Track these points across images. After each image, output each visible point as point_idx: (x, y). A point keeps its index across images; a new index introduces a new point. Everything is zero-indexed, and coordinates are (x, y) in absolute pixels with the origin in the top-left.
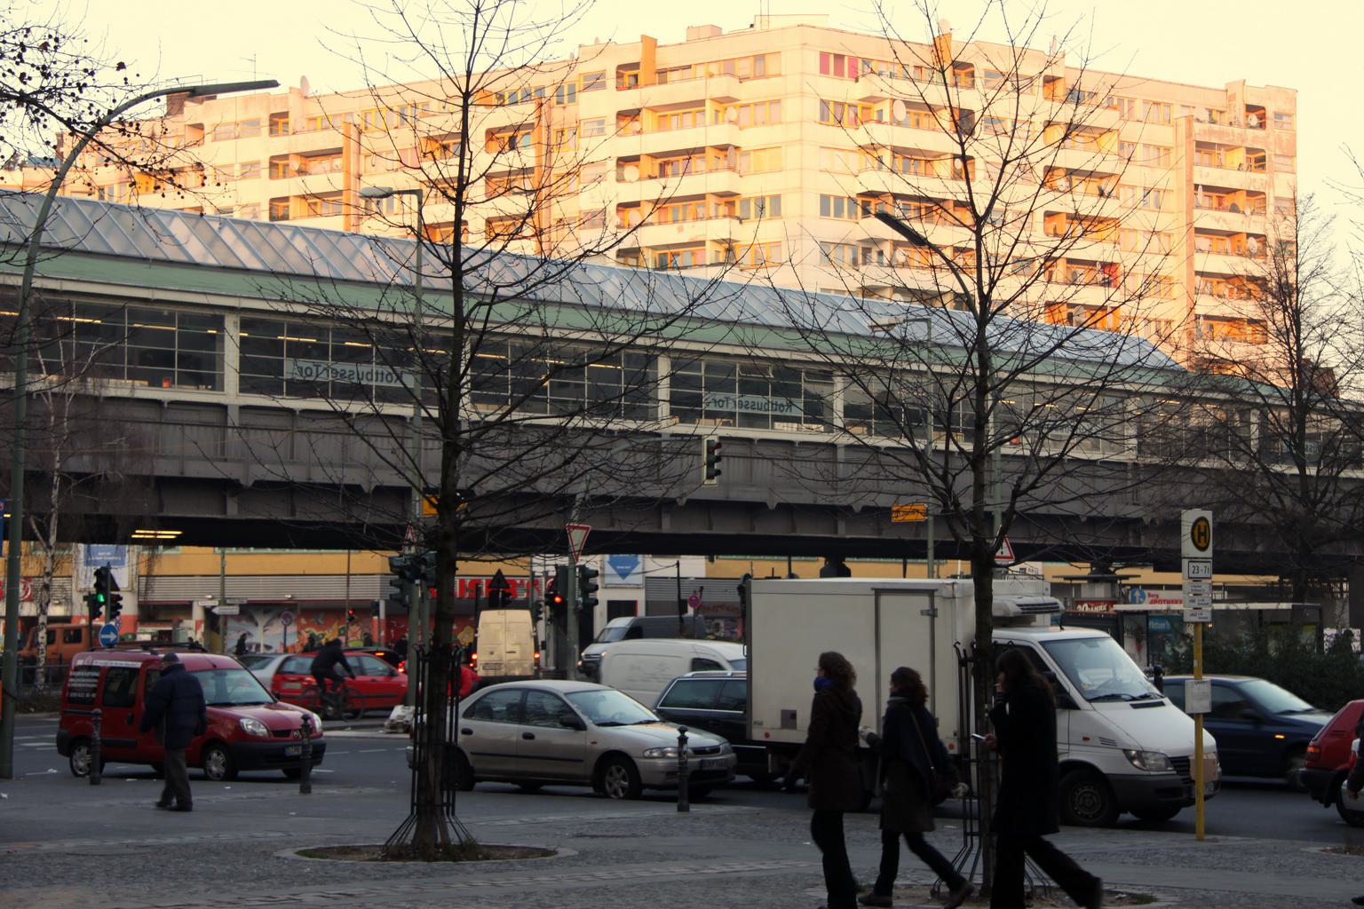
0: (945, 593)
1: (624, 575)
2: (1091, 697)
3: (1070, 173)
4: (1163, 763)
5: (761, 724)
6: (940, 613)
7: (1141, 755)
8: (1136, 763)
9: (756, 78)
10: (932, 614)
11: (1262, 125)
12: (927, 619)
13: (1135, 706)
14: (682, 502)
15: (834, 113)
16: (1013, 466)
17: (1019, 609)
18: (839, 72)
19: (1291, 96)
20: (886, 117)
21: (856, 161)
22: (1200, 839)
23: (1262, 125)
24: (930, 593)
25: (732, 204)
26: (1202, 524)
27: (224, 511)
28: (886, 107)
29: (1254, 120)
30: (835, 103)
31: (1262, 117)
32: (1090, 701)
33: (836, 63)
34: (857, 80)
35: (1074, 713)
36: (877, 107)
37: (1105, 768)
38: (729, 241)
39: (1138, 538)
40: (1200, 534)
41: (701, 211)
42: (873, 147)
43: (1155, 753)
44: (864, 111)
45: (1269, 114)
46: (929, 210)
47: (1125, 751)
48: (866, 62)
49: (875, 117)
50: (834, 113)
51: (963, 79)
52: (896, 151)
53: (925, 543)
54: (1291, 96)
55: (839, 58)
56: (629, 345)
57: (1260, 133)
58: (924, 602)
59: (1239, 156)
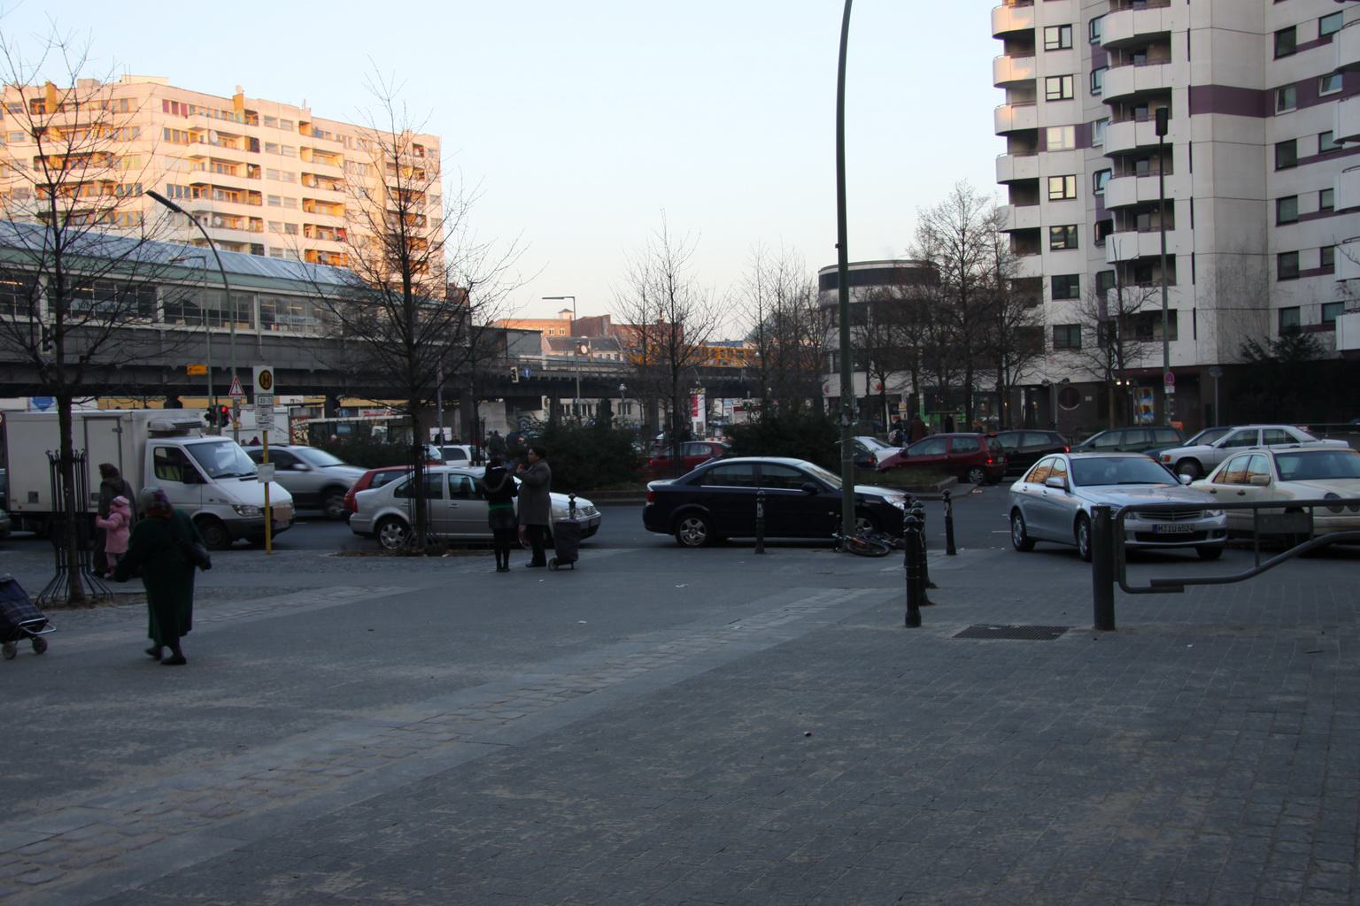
0: (126, 419)
1: (43, 408)
2: (215, 475)
3: (317, 177)
4: (256, 512)
5: (15, 501)
6: (124, 430)
7: (243, 507)
8: (240, 512)
9: (122, 112)
10: (119, 431)
11: (422, 155)
12: (116, 434)
13: (241, 480)
14: (312, 371)
15: (171, 135)
16: (96, 333)
17: (174, 426)
18: (175, 112)
19: (437, 141)
20: (206, 140)
21: (188, 165)
22: (269, 554)
23: (422, 155)
24: (117, 418)
25: (111, 187)
26: (266, 374)
27: (161, 380)
28: (205, 134)
29: (417, 153)
30: (174, 130)
31: (422, 151)
32: (214, 478)
33: (172, 106)
34: (186, 117)
35: (204, 486)
36: (200, 134)
37: (222, 516)
38: (307, 237)
39: (344, 382)
40: (265, 380)
41: (92, 191)
42: (197, 158)
43: (251, 506)
44: (193, 135)
45: (425, 150)
46: (234, 195)
47: (233, 506)
48: (192, 107)
49: (199, 139)
50: (171, 135)
51: (252, 121)
52: (213, 160)
53: (207, 387)
54: (437, 141)
55: (175, 103)
56: (101, 277)
57: (420, 159)
58: (114, 424)
59: (242, 143)
